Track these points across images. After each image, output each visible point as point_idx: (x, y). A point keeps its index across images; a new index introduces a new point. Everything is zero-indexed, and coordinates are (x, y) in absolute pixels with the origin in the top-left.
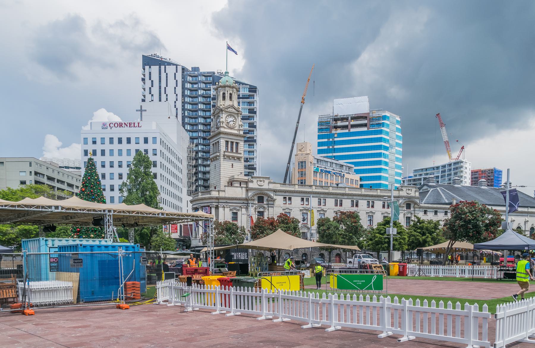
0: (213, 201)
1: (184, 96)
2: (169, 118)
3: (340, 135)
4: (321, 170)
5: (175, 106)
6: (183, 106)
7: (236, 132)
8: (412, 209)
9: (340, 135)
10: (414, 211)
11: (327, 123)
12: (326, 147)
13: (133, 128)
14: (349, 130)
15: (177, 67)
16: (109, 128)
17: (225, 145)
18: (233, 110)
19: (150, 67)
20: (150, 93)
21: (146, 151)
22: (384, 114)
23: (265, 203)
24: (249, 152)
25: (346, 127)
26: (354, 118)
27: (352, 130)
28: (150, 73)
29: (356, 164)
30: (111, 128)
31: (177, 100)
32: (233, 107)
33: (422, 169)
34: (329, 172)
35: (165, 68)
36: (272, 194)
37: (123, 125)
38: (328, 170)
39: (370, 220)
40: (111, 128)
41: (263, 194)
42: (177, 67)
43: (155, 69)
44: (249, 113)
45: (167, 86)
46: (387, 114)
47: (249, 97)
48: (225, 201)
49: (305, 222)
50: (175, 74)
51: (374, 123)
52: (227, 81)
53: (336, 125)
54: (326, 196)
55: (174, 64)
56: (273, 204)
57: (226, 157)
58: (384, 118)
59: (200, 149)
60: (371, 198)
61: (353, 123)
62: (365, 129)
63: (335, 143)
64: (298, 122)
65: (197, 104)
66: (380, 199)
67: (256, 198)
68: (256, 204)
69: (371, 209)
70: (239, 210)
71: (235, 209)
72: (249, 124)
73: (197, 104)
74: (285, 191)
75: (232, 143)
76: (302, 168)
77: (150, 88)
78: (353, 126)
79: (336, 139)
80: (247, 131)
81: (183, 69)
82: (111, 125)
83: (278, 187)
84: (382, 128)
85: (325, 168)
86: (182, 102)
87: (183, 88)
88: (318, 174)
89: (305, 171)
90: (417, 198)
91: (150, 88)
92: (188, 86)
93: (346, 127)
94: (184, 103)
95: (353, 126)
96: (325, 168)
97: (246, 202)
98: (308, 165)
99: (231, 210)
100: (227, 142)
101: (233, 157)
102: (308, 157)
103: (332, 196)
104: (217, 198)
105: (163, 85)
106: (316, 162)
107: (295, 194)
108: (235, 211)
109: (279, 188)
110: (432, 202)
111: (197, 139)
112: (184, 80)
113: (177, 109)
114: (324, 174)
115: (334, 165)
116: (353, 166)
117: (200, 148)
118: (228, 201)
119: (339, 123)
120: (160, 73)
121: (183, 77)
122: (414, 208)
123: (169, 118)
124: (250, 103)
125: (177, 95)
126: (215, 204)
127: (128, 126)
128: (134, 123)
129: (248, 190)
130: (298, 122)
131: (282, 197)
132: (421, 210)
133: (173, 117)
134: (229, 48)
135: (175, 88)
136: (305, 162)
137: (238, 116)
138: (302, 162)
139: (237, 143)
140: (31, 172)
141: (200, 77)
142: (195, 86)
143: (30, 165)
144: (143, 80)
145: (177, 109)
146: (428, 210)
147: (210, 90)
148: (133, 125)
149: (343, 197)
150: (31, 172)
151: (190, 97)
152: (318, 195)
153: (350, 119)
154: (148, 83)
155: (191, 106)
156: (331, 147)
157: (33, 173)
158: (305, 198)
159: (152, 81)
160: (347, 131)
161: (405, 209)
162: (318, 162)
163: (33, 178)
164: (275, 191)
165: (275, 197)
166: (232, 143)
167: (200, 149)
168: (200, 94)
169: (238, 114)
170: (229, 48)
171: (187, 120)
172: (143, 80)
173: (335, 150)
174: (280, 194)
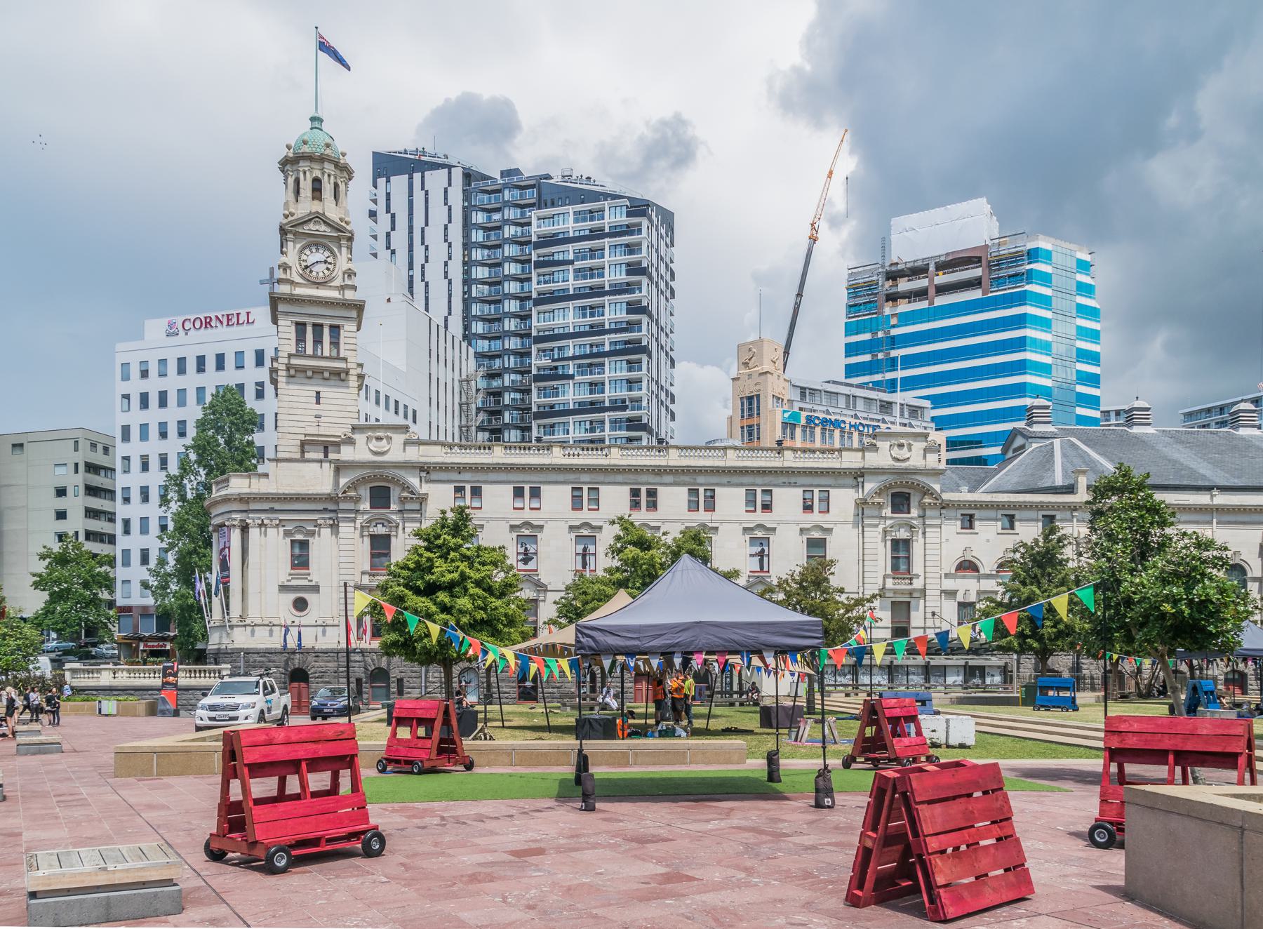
0: (235, 506)
1: (467, 246)
2: (389, 300)
3: (906, 318)
4: (809, 419)
5: (446, 273)
6: (467, 272)
7: (334, 294)
8: (914, 512)
9: (906, 318)
10: (923, 517)
11: (872, 286)
12: (867, 358)
13: (235, 328)
14: (931, 303)
15: (450, 173)
16: (182, 332)
17: (293, 336)
18: (323, 227)
19: (388, 181)
20: (388, 248)
21: (241, 387)
22: (1030, 246)
23: (394, 507)
24: (629, 381)
25: (921, 294)
26: (943, 266)
27: (940, 301)
28: (388, 195)
29: (938, 401)
30: (187, 332)
31: (450, 258)
32: (319, 218)
33: (1209, 410)
34: (837, 424)
35: (423, 177)
36: (414, 481)
37: (213, 324)
38: (833, 418)
39: (761, 555)
40: (187, 332)
41: (386, 480)
42: (450, 173)
43: (399, 183)
44: (629, 273)
45: (427, 224)
46: (1044, 244)
47: (629, 230)
48: (266, 506)
49: (531, 565)
50: (446, 191)
51: (1003, 273)
52: (305, 143)
53: (894, 290)
54: (601, 478)
55: (442, 166)
56: (419, 511)
57: (292, 372)
58: (1033, 255)
59: (507, 384)
60: (759, 480)
61: (942, 279)
62: (976, 294)
63: (894, 342)
64: (800, 295)
65: (499, 265)
66: (793, 480)
67: (365, 492)
68: (364, 513)
69: (760, 517)
70: (312, 534)
71: (299, 529)
72: (628, 303)
73: (499, 265)
74: (460, 468)
75: (318, 328)
76: (750, 416)
77: (388, 235)
78: (942, 290)
79: (894, 332)
80: (624, 325)
81: (468, 176)
82: (188, 325)
83: (436, 455)
84: (1028, 287)
85: (828, 412)
86: (464, 263)
87: (467, 226)
88: (798, 431)
89: (758, 425)
90: (936, 473)
91: (388, 235)
92: (479, 218)
93: (921, 294)
94: (468, 264)
95: (942, 290)
96: (828, 412)
97: (331, 507)
98: (768, 403)
99: (287, 533)
100: (300, 327)
101: (318, 372)
102: (766, 381)
103: (620, 478)
104: (243, 499)
105: (419, 221)
106: (796, 395)
107: (493, 476)
108: (299, 537)
109: (439, 460)
110: (1010, 488)
111: (499, 356)
112: (470, 203)
113: (450, 282)
114: (818, 430)
115: (860, 405)
116: (927, 403)
117: (507, 380)
118: (277, 506)
119: (904, 285)
120: (411, 194)
121: (467, 195)
122: (923, 507)
123: (389, 300)
124: (631, 249)
125: (450, 245)
126: (238, 516)
127: (225, 322)
128: (238, 315)
129: (339, 468)
130: (800, 295)
131: (451, 487)
132: (951, 513)
133: (399, 299)
134: (324, 47)
135: (446, 228)
136: (758, 396)
137: (340, 248)
138: (750, 399)
139: (335, 329)
140: (76, 465)
141: (506, 192)
142: (496, 216)
143: (76, 449)
144: (373, 214)
145: (450, 282)
146: (977, 514)
147: (529, 224)
148: (235, 320)
149: (658, 479)
150: (76, 465)
151: (483, 247)
152: (571, 477)
153: (932, 268)
154: (384, 219)
155: (486, 269)
156: (880, 356)
157: (81, 468)
158: (527, 487)
159: (393, 216)
160: (924, 305)
161: (887, 511)
162: (803, 395)
163: (80, 479)
164: (425, 470)
165: (425, 489)
166: (318, 328)
167: (507, 384)
168: (506, 236)
169: (339, 238)
170: (324, 47)
171: (476, 309)
172: (373, 214)
173: (892, 364)
174: (443, 476)
